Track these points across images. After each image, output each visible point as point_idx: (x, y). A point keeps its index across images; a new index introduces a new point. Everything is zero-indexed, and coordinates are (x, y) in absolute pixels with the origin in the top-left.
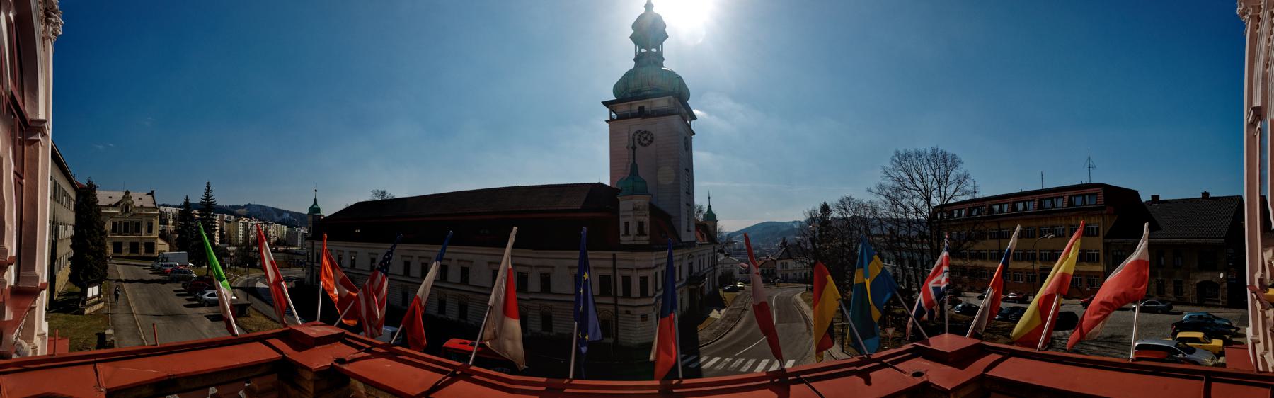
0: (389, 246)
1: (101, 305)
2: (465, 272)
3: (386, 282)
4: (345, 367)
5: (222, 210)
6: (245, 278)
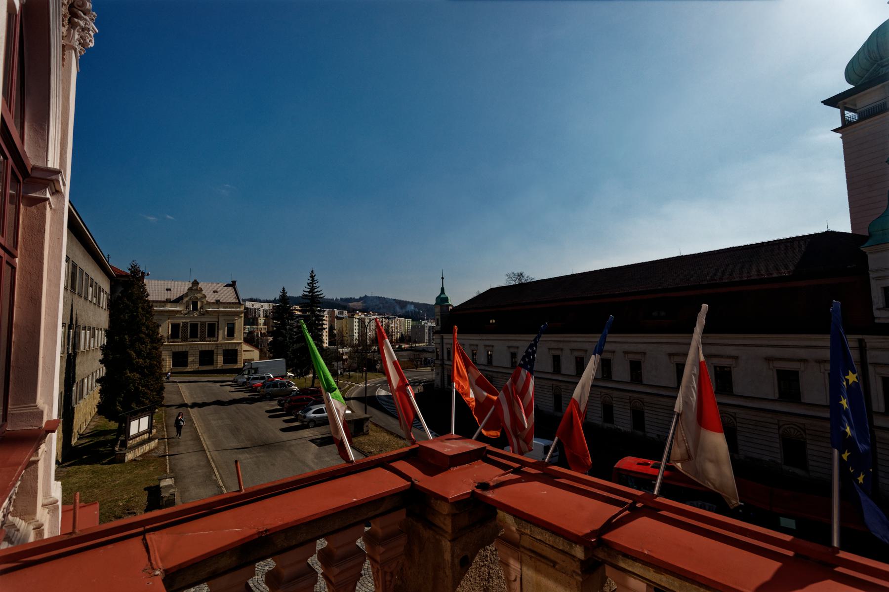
0: (532, 337)
1: (153, 444)
2: (636, 368)
3: (532, 382)
4: (490, 494)
5: (332, 304)
6: (362, 385)
